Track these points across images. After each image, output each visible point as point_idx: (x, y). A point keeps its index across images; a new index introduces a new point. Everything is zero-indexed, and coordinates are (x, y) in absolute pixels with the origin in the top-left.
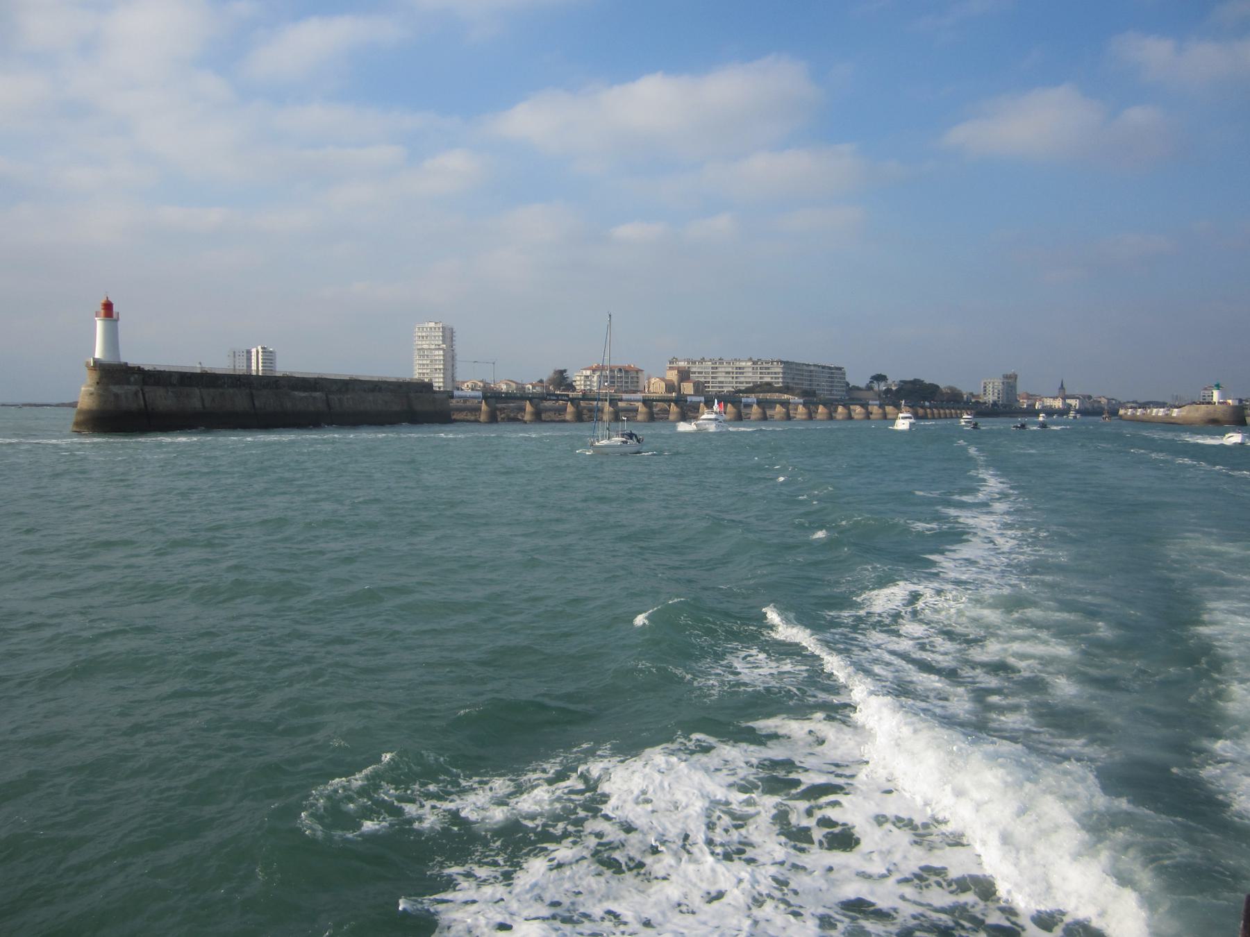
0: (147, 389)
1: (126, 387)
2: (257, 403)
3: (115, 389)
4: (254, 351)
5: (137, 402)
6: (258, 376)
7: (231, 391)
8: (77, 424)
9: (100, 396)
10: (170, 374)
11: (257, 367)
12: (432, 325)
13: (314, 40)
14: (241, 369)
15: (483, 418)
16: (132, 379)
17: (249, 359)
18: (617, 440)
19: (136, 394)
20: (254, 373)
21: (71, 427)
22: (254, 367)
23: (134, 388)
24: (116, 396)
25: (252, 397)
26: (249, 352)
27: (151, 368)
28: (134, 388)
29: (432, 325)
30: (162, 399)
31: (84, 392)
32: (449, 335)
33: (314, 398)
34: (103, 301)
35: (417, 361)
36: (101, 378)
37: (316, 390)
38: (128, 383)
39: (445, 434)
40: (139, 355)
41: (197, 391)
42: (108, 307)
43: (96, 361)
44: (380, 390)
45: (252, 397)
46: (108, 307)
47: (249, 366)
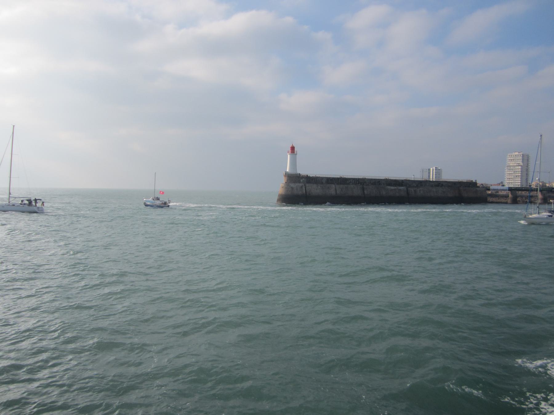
0: (307, 185)
1: (297, 184)
2: (365, 192)
3: (292, 185)
4: (431, 169)
5: (304, 191)
6: (433, 181)
7: (352, 186)
8: (278, 200)
9: (286, 188)
10: (322, 178)
11: (433, 178)
12: (517, 153)
13: (480, 21)
14: (425, 178)
15: (509, 201)
16: (302, 181)
17: (429, 173)
18: (545, 214)
19: (302, 187)
20: (431, 180)
21: (276, 202)
22: (431, 177)
23: (301, 185)
24: (292, 188)
25: (363, 189)
26: (429, 170)
27: (384, 178)
28: (301, 185)
29: (517, 153)
30: (315, 190)
31: (279, 186)
32: (526, 159)
33: (400, 190)
34: (291, 146)
35: (507, 172)
36: (287, 180)
37: (402, 185)
38: (300, 182)
39: (474, 210)
40: (303, 171)
41: (333, 186)
42: (293, 148)
43: (286, 173)
44: (442, 185)
45: (363, 189)
46: (293, 148)
47: (429, 176)
